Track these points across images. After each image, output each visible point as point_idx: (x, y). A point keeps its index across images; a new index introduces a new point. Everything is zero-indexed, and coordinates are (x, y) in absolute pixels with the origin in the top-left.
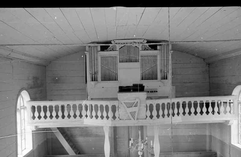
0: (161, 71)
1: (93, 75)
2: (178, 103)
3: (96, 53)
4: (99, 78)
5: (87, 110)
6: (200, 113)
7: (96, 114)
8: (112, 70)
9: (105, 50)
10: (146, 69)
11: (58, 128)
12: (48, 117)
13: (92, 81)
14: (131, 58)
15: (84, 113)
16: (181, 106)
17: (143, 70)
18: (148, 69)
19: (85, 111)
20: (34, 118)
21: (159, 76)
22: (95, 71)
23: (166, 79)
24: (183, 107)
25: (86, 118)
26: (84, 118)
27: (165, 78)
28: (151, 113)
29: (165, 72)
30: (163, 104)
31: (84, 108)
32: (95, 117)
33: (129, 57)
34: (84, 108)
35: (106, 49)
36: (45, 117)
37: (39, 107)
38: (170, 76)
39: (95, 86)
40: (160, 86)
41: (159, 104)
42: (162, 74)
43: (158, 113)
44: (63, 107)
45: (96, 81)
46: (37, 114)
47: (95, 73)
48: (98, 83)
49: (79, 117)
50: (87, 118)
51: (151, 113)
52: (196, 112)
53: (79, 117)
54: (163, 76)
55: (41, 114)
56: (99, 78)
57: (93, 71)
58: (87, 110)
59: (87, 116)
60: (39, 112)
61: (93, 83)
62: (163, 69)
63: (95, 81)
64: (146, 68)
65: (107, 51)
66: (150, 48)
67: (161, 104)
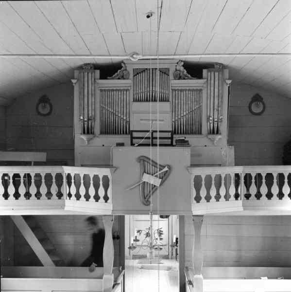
0: (208, 119)
1: (86, 123)
2: (97, 178)
3: (92, 84)
4: (97, 130)
5: (69, 184)
6: (256, 196)
7: (77, 190)
8: (119, 115)
9: (108, 78)
10: (182, 115)
11: (22, 216)
12: (253, 196)
13: (84, 133)
14: (154, 94)
15: (65, 189)
16: (242, 181)
17: (177, 115)
18: (185, 114)
19: (67, 187)
20: (6, 196)
21: (205, 130)
22: (90, 115)
23: (217, 133)
24: (245, 183)
25: (68, 198)
26: (65, 198)
27: (215, 131)
28: (237, 190)
29: (216, 120)
30: (209, 178)
31: (65, 180)
32: (216, 197)
33: (151, 92)
34: (65, 180)
35: (110, 76)
36: (17, 196)
37: (269, 176)
38: (224, 127)
39: (88, 143)
40: (103, 145)
41: (200, 176)
42: (210, 124)
43: (227, 192)
44: (237, 175)
45: (91, 133)
46: (11, 190)
47: (89, 119)
48: (94, 137)
49: (45, 197)
50: (71, 198)
51: (248, 190)
52: (18, 193)
53: (57, 196)
54: (212, 128)
55: (41, 189)
56: (97, 130)
57: (86, 116)
58: (69, 184)
59: (70, 195)
60: (269, 185)
61: (84, 137)
62: (212, 115)
63: (88, 133)
64: (182, 112)
65: (113, 79)
66: (189, 76)
67: (265, 175)
